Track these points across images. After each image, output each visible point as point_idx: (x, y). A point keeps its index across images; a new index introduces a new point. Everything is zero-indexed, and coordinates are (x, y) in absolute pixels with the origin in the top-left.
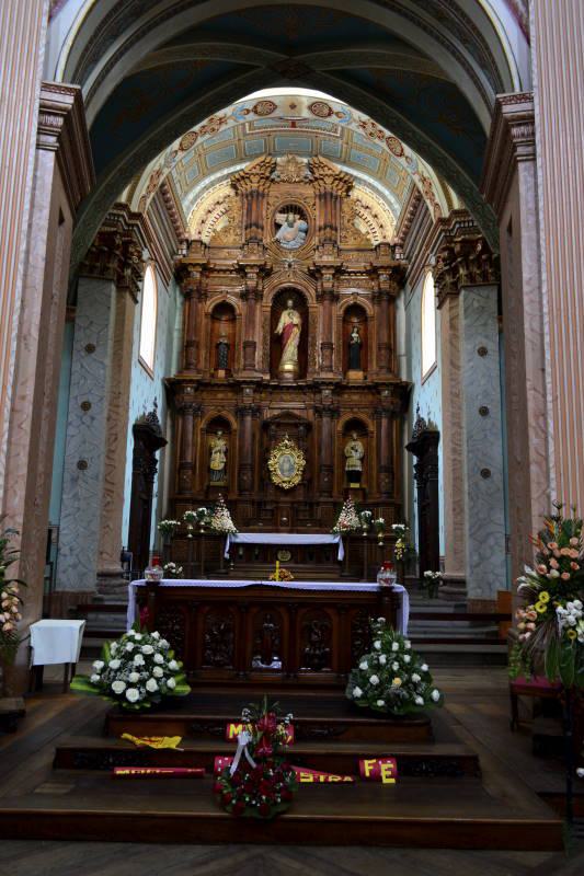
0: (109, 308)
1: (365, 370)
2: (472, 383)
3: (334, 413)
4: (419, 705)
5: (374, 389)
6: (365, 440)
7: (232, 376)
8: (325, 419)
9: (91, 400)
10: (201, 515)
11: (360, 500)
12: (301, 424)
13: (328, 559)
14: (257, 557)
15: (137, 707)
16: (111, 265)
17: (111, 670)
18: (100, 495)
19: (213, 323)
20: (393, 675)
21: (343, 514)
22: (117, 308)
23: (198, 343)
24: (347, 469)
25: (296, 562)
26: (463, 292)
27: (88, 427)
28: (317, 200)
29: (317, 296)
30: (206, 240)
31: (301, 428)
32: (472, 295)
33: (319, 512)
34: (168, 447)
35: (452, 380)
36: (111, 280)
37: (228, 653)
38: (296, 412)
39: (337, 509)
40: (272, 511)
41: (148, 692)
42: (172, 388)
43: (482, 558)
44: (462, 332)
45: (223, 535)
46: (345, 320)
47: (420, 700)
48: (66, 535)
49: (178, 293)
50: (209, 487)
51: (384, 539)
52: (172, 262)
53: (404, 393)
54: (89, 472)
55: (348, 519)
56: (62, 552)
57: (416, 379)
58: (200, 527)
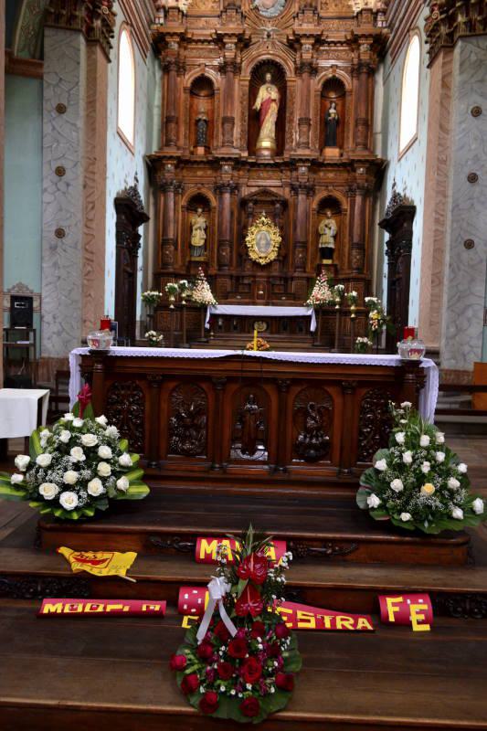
0: (78, 63)
1: (341, 147)
2: (462, 148)
3: (310, 191)
4: (458, 520)
5: (349, 166)
6: (338, 218)
7: (211, 153)
8: (300, 197)
9: (65, 166)
10: (182, 287)
11: (332, 276)
12: (278, 201)
13: (301, 330)
14: (235, 328)
15: (75, 516)
16: (77, 13)
17: (40, 467)
18: (81, 266)
19: (192, 97)
20: (422, 479)
21: (316, 289)
22: (88, 65)
23: (178, 118)
24: (320, 246)
25: (271, 333)
26: (460, 43)
27: (64, 193)
29: (296, 69)
30: (183, 8)
31: (278, 205)
32: (470, 47)
33: (293, 286)
34: (151, 222)
35: (439, 145)
36: (80, 31)
37: (200, 441)
38: (272, 189)
39: (310, 283)
40: (249, 285)
41: (89, 496)
42: (153, 165)
43: (459, 330)
44: (455, 92)
45: (203, 307)
46: (323, 95)
47: (458, 513)
48: (48, 303)
49: (157, 67)
50: (190, 262)
51: (357, 312)
52: (150, 32)
53: (379, 170)
54: (68, 240)
55: (321, 292)
56: (45, 319)
57: (392, 155)
58: (182, 299)
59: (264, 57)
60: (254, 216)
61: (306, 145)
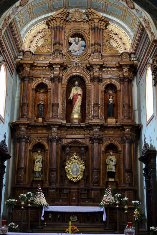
8: (95, 144)
25: (80, 222)
28: (91, 31)
29: (91, 80)
40: (67, 193)
59: (74, 74)
60: (69, 155)
61: (98, 117)
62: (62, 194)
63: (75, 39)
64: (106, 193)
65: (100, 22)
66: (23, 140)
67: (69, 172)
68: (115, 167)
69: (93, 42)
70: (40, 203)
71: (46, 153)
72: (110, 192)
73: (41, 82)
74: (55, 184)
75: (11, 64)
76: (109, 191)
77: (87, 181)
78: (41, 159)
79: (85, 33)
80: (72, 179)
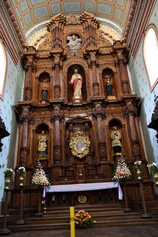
3: (104, 117)
5: (122, 102)
6: (121, 130)
8: (98, 119)
14: (64, 202)
21: (119, 168)
25: (91, 204)
28: (85, 30)
29: (89, 66)
31: (86, 125)
33: (101, 170)
39: (113, 168)
40: (73, 171)
45: (40, 188)
59: (73, 63)
60: (73, 132)
61: (99, 94)
62: (68, 172)
63: (72, 37)
64: (119, 164)
65: (93, 22)
66: (26, 120)
67: (73, 148)
68: (121, 142)
69: (88, 37)
70: (39, 183)
71: (50, 133)
72: (123, 162)
73: (44, 71)
74: (60, 162)
75: (10, 46)
76: (122, 161)
77: (93, 158)
78: (46, 139)
79: (80, 33)
80: (77, 156)
